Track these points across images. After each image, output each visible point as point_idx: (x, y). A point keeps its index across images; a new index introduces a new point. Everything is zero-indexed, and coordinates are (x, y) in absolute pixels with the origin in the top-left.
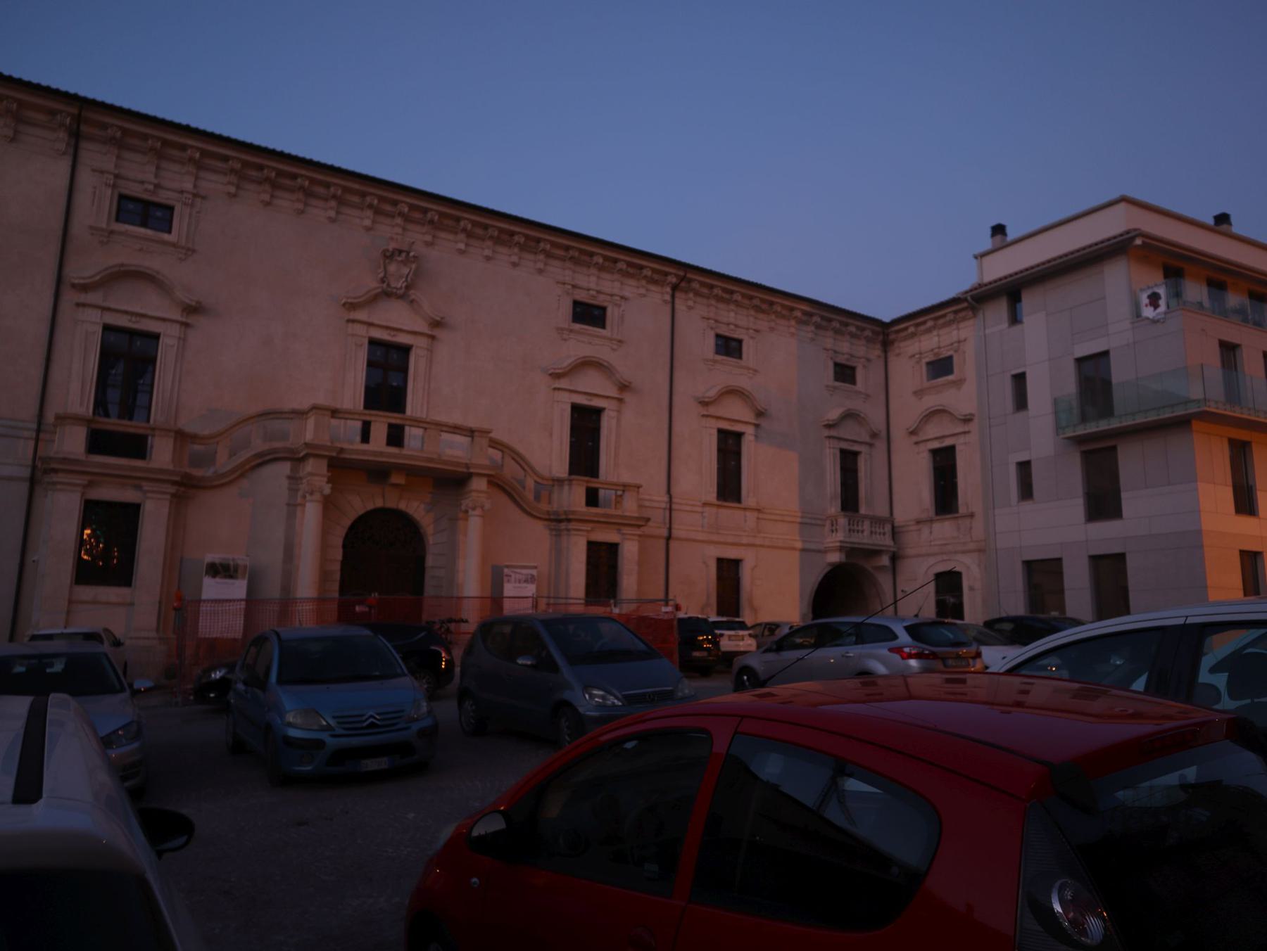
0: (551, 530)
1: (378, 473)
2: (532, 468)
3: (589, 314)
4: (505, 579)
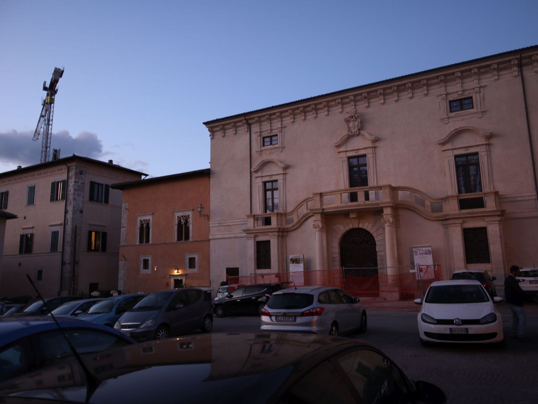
1: (344, 214)
3: (461, 104)
4: (414, 254)
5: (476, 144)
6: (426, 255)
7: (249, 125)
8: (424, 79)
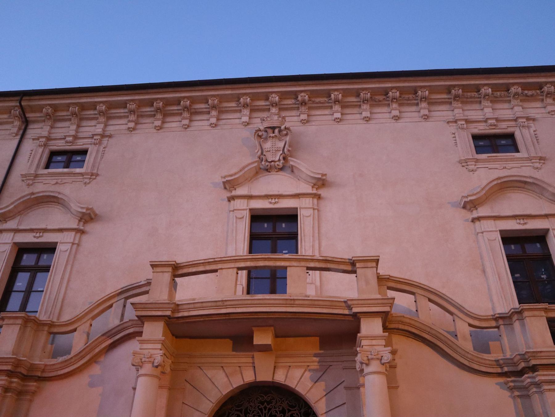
0: (511, 389)
1: (235, 332)
2: (460, 309)
5: (543, 213)
7: (26, 123)
8: (424, 87)
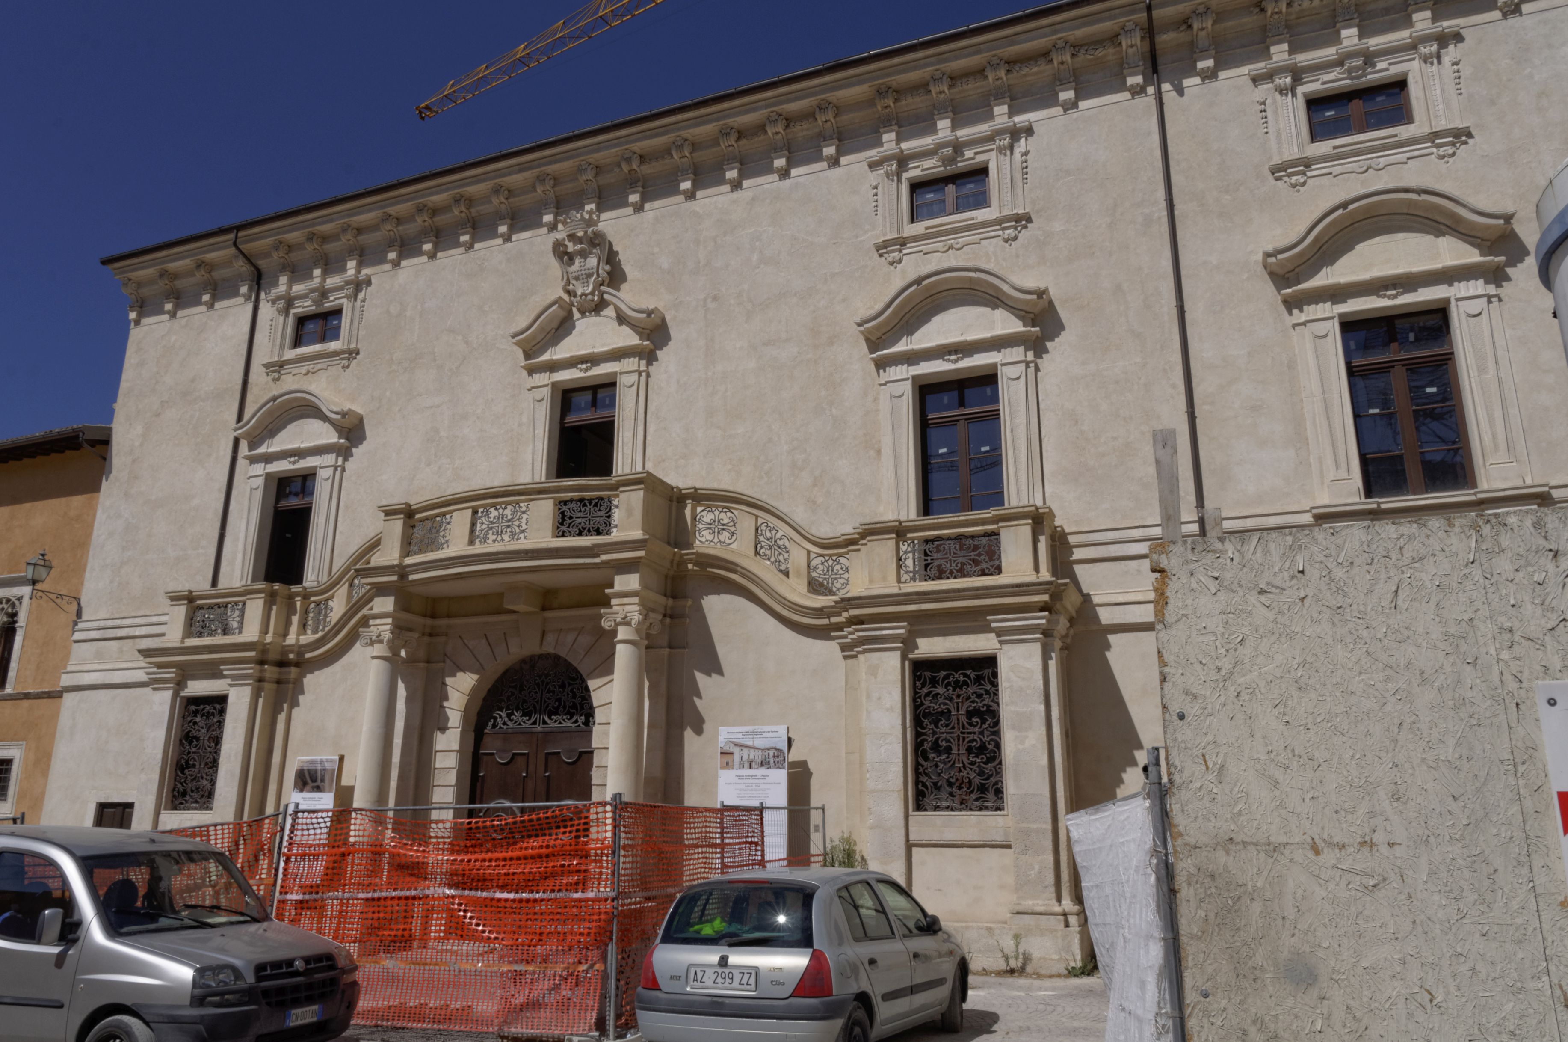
6: (762, 771)
